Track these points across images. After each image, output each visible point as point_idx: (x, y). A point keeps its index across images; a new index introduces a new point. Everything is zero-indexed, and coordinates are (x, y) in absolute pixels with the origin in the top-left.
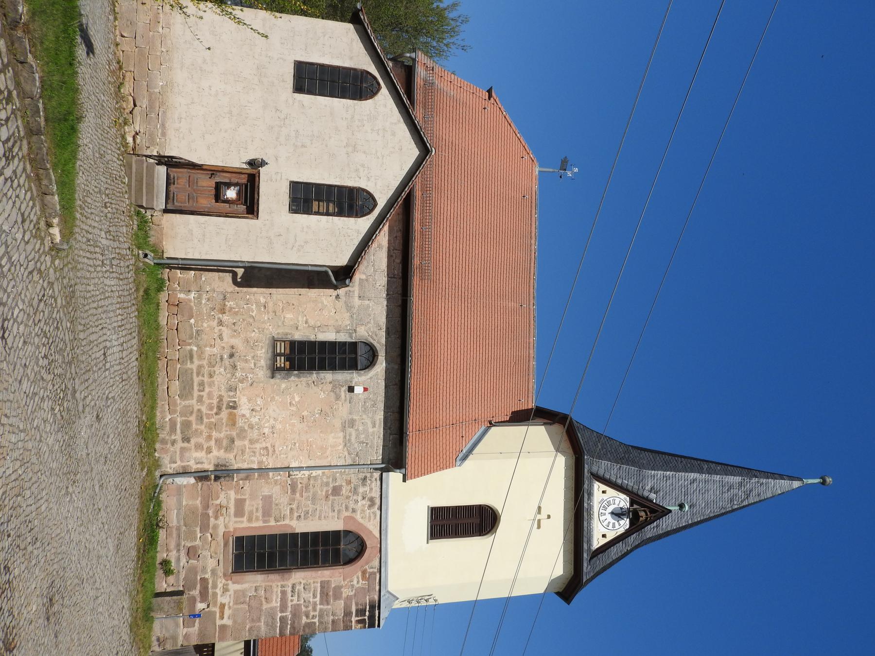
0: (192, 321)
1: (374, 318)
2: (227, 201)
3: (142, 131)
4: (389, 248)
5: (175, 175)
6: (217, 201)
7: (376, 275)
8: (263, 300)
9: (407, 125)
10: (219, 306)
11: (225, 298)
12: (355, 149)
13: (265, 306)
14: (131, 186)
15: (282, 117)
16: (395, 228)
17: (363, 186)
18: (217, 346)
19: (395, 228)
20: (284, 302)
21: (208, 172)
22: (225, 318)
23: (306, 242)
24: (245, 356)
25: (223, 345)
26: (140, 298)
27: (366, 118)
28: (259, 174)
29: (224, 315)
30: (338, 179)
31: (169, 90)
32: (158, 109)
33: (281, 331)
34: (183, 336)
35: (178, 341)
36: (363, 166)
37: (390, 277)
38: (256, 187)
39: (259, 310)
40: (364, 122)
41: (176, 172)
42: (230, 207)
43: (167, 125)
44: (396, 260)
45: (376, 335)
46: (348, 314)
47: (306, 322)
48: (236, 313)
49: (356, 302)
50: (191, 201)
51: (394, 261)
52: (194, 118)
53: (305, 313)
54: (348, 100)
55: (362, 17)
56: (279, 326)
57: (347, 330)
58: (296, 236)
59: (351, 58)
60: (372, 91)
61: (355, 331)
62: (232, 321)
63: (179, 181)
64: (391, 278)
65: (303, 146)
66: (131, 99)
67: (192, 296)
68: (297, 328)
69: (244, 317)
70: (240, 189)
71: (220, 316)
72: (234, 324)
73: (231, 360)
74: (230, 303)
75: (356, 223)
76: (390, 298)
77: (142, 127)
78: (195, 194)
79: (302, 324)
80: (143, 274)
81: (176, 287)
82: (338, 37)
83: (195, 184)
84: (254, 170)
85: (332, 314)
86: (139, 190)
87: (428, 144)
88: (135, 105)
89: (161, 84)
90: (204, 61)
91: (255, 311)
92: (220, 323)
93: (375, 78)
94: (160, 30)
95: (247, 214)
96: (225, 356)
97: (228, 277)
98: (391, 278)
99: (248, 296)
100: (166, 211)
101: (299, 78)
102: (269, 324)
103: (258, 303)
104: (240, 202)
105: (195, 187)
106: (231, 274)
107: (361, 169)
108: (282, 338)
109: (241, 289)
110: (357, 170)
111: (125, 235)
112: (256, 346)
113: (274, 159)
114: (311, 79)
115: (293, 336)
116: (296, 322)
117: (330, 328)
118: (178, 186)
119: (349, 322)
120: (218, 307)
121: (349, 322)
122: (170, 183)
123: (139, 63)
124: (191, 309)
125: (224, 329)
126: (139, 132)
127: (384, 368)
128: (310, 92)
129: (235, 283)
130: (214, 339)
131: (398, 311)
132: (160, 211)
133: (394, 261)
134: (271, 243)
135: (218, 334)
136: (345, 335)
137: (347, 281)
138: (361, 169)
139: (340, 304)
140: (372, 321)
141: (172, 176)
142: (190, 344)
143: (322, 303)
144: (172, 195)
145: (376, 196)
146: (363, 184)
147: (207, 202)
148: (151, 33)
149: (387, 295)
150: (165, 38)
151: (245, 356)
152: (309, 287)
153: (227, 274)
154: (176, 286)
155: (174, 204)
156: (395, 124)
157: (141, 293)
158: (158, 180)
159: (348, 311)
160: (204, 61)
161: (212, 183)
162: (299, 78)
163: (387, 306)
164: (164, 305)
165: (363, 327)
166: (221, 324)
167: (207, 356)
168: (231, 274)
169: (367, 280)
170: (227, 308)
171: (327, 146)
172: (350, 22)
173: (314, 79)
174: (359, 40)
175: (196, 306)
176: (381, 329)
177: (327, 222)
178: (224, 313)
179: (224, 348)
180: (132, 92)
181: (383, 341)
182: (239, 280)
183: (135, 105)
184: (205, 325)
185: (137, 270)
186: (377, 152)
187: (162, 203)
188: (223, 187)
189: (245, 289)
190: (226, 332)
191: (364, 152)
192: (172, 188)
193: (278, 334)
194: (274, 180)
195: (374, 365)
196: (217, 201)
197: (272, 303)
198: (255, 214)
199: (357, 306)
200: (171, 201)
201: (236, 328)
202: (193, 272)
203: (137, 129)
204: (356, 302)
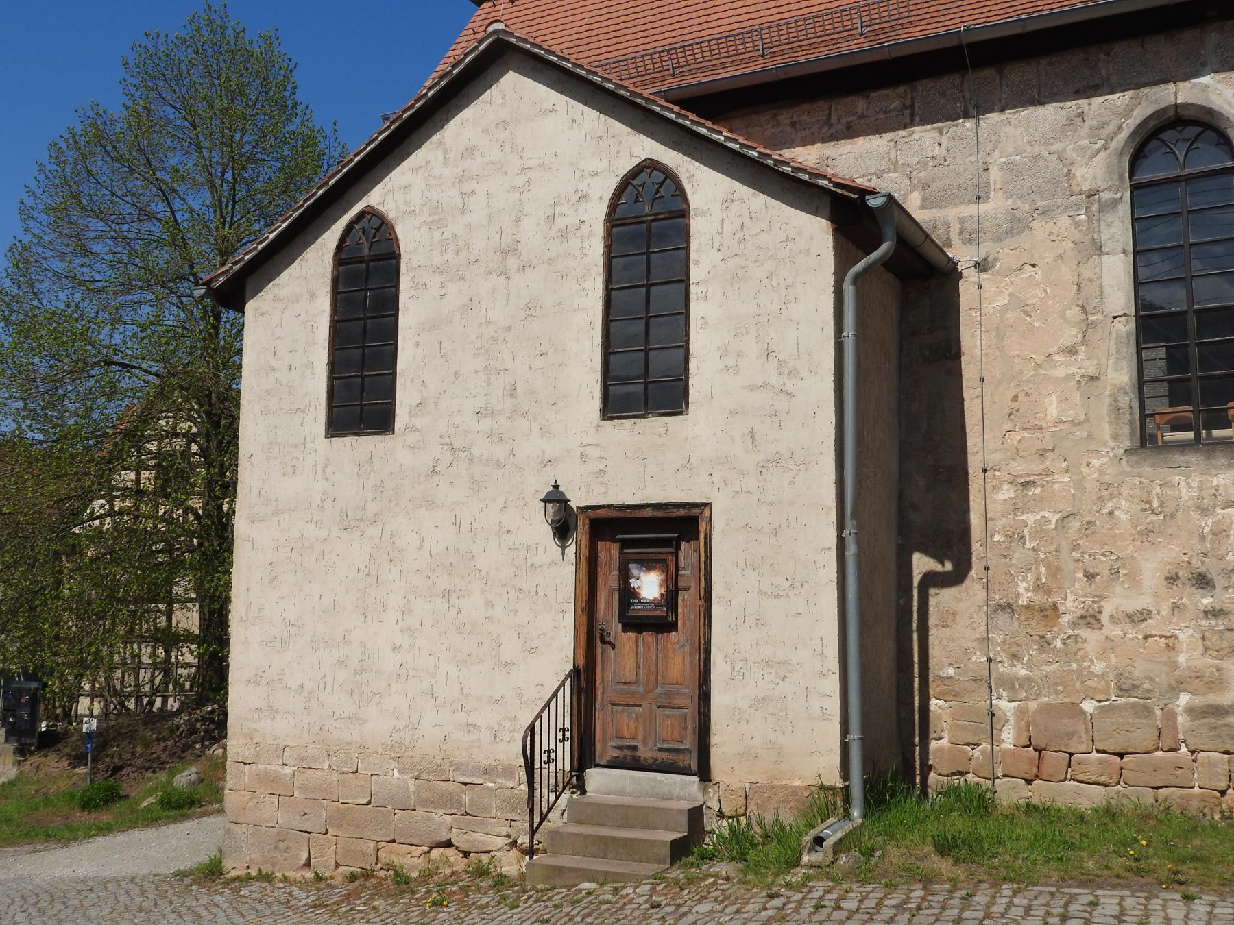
0: (1089, 706)
1: (1046, 142)
2: (671, 597)
3: (505, 830)
4: (824, 140)
5: (613, 744)
6: (673, 627)
7: (909, 160)
8: (1007, 493)
9: (448, 121)
10: (1033, 623)
11: (1007, 607)
12: (511, 250)
13: (1027, 484)
14: (607, 873)
15: (447, 456)
16: (768, 133)
17: (601, 210)
18: (1170, 629)
19: (768, 133)
20: (1009, 426)
21: (599, 651)
22: (1071, 605)
23: (768, 353)
24: (1203, 538)
25: (1165, 609)
26: (960, 872)
27: (437, 235)
28: (588, 508)
29: (1062, 609)
30: (589, 285)
31: (410, 753)
32: (451, 786)
33: (1106, 430)
34: (1142, 737)
35: (1159, 753)
36: (551, 220)
37: (909, 117)
38: (621, 515)
39: (1039, 501)
40: (445, 236)
41: (604, 742)
42: (688, 589)
43: (486, 762)
44: (859, 111)
45: (1103, 125)
46: (1035, 224)
47: (1071, 351)
48: (1055, 571)
49: (995, 206)
50: (677, 702)
51: (862, 117)
52: (465, 691)
53: (1039, 358)
54: (402, 287)
55: (222, 279)
56: (1090, 437)
57: (1090, 220)
58: (752, 388)
59: (313, 295)
60: (378, 229)
61: (1091, 195)
62: (1080, 584)
63: (626, 734)
64: (912, 116)
65: (513, 393)
66: (436, 853)
67: (1004, 705)
68: (1093, 379)
69: (1065, 546)
70: (635, 561)
71: (1065, 619)
72: (1090, 576)
73: (1220, 582)
74: (1022, 591)
75: (704, 212)
76: (977, 107)
77: (497, 830)
78: (659, 690)
79: (1083, 365)
80: (882, 857)
81: (983, 752)
82: (273, 334)
83: (633, 687)
84: (580, 523)
85: (1038, 274)
86: (630, 849)
87: (482, 47)
88: (448, 844)
89: (396, 774)
90: (342, 663)
91: (1045, 513)
92: (1090, 619)
93: (349, 228)
94: (288, 770)
95: (698, 538)
96: (1207, 601)
97: (940, 599)
98: (912, 116)
99: (997, 538)
100: (704, 774)
101: (361, 420)
102: (1085, 470)
103: (1016, 508)
104: (669, 558)
105: (641, 690)
106: (932, 591)
107: (560, 223)
108: (1131, 423)
109: (974, 559)
110: (563, 234)
111: (719, 908)
112: (1162, 505)
113: (548, 468)
114: (362, 391)
115: (1121, 389)
116: (1072, 384)
117: (1087, 274)
118: (640, 737)
119: (1064, 221)
120: (1036, 628)
121: (1064, 221)
122: (635, 759)
123: (357, 827)
124: (1047, 710)
125: (1108, 608)
126: (508, 836)
127: (1222, 75)
128: (389, 392)
129: (957, 577)
130: (1146, 638)
131: (1018, 73)
132: (705, 792)
133: (862, 117)
134: (778, 461)
135: (1128, 627)
136: (1109, 225)
137: (874, 202)
138: (560, 223)
139: (1005, 256)
140: (1057, 146)
141: (616, 753)
142: (1171, 716)
143: (1004, 308)
144: (665, 755)
145: (626, 165)
146: (597, 212)
147: (677, 647)
148: (296, 793)
149: (966, 115)
150: (302, 760)
151: (1203, 538)
152: (957, 355)
153: (932, 601)
154: (977, 753)
155: (688, 751)
156: (446, 151)
157: (944, 866)
158: (622, 793)
159: (1026, 227)
160: (342, 663)
161: (627, 640)
162: (361, 420)
163: (1002, 110)
164: (1040, 793)
165: (1079, 172)
166: (1093, 616)
167: (1208, 661)
168: (932, 591)
169: (925, 186)
170: (1039, 599)
171: (509, 329)
172: (241, 309)
173: (363, 384)
174: (276, 281)
175: (1038, 696)
176: (1081, 115)
177: (705, 298)
178: (1055, 607)
179: (1175, 607)
180: (419, 850)
181: (1120, 99)
182: (949, 566)
183: (448, 844)
184: (1099, 667)
185: (861, 876)
186: (514, 189)
187: (683, 784)
188: (635, 610)
189: (976, 547)
190: (1117, 602)
191: (518, 222)
192: (645, 753)
193: (1115, 437)
194: (602, 467)
195: (1210, 112)
196: (673, 627)
197: (1013, 464)
198: (695, 512)
199: (1010, 202)
200: (681, 757)
201: (1104, 570)
202: (934, 703)
203: (501, 842)
204: (995, 206)
